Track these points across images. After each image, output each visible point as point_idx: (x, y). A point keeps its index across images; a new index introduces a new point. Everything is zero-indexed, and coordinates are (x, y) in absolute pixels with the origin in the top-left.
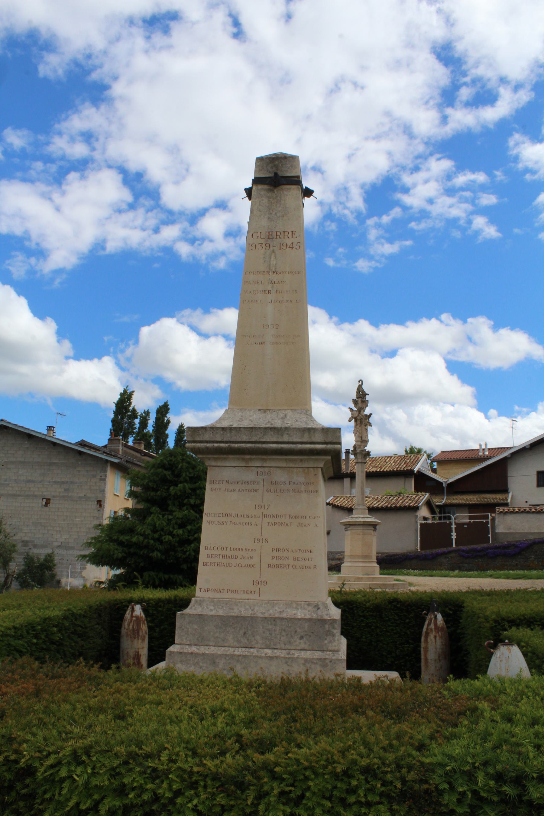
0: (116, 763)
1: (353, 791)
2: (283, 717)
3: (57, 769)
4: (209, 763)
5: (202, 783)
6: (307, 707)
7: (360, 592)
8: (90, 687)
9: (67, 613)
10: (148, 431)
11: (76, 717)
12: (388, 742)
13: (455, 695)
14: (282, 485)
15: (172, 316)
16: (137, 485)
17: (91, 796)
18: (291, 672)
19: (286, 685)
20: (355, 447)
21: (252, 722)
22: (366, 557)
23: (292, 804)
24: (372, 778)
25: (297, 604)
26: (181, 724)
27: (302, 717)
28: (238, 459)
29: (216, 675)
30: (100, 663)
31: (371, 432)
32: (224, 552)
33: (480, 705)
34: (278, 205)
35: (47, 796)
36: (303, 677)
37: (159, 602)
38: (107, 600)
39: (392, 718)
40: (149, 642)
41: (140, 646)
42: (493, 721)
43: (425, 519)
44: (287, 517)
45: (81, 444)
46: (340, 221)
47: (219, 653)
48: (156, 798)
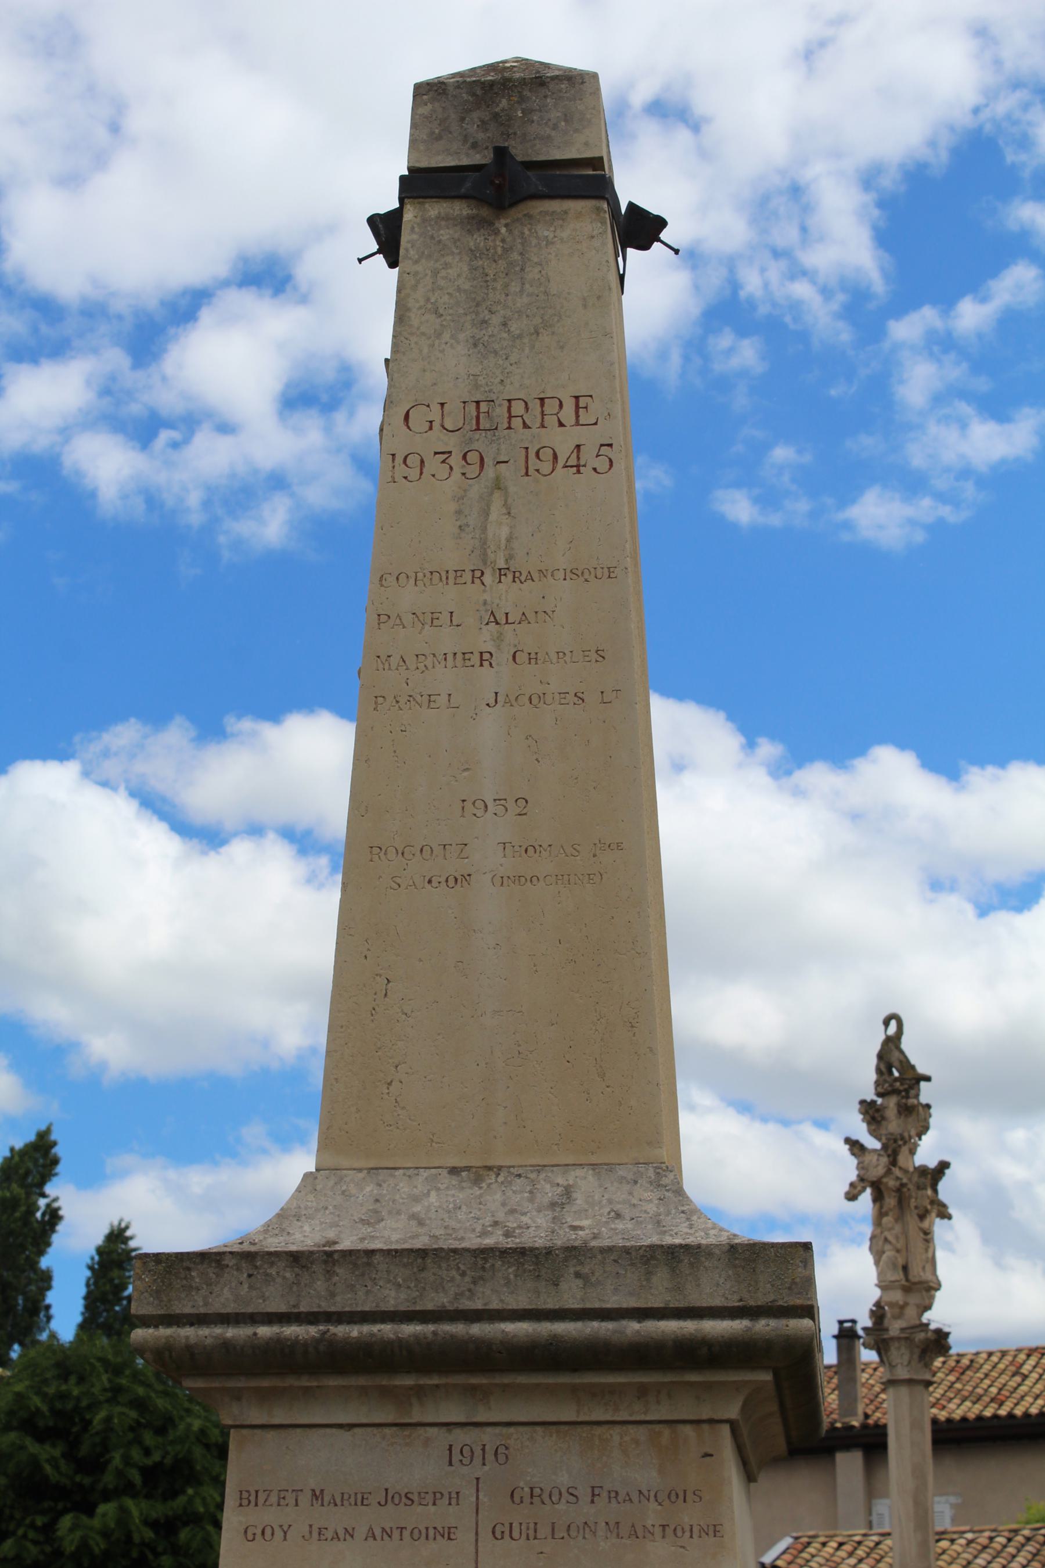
14: (562, 1506)
15: (62, 756)
20: (878, 1313)
28: (363, 1391)
31: (949, 1237)
34: (514, 287)
46: (777, 329)
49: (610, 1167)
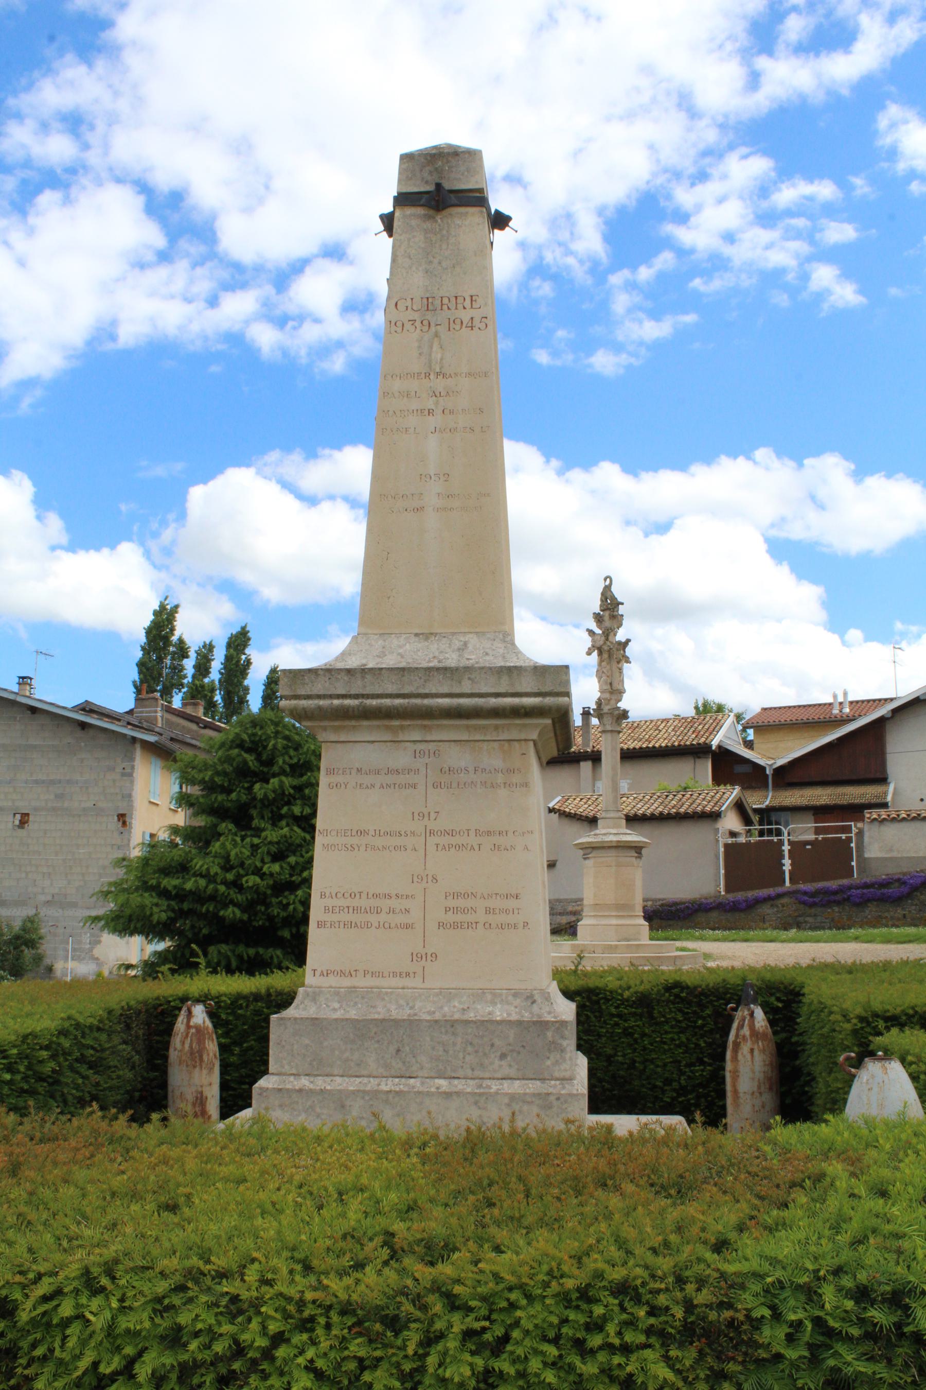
0: (162, 1287)
1: (596, 1326)
2: (471, 1198)
3: (54, 1303)
4: (334, 1284)
5: (322, 1320)
6: (514, 1179)
7: (611, 970)
8: (112, 1155)
9: (67, 1024)
10: (213, 681)
11: (88, 1210)
12: (660, 1238)
13: (785, 1152)
15: (248, 466)
16: (192, 782)
17: (119, 1349)
18: (485, 1120)
19: (474, 1142)
20: (599, 703)
21: (413, 1209)
22: (623, 908)
23: (487, 1353)
24: (632, 1303)
25: (494, 995)
26: (282, 1217)
27: (504, 1197)
29: (344, 1127)
30: (130, 1112)
32: (356, 902)
33: (831, 1168)
34: (444, 247)
35: (39, 1352)
36: (506, 1128)
37: (237, 1000)
38: (141, 999)
39: (669, 1196)
40: (222, 1074)
41: (205, 1081)
42: (853, 1195)
43: (733, 834)
44: (472, 833)
45: (83, 710)
46: (557, 277)
47: (351, 1088)
48: (239, 1350)
49: (484, 633)
